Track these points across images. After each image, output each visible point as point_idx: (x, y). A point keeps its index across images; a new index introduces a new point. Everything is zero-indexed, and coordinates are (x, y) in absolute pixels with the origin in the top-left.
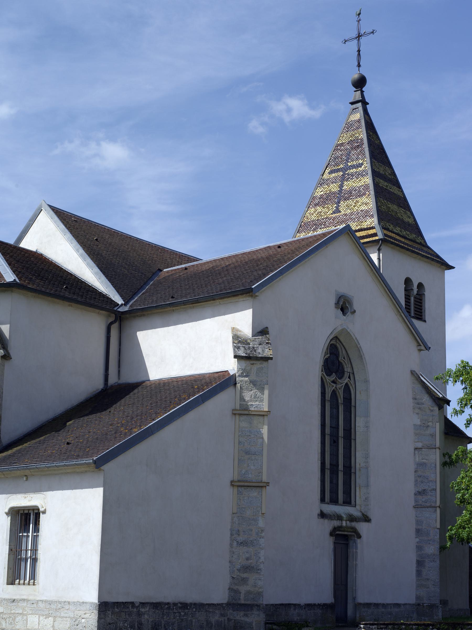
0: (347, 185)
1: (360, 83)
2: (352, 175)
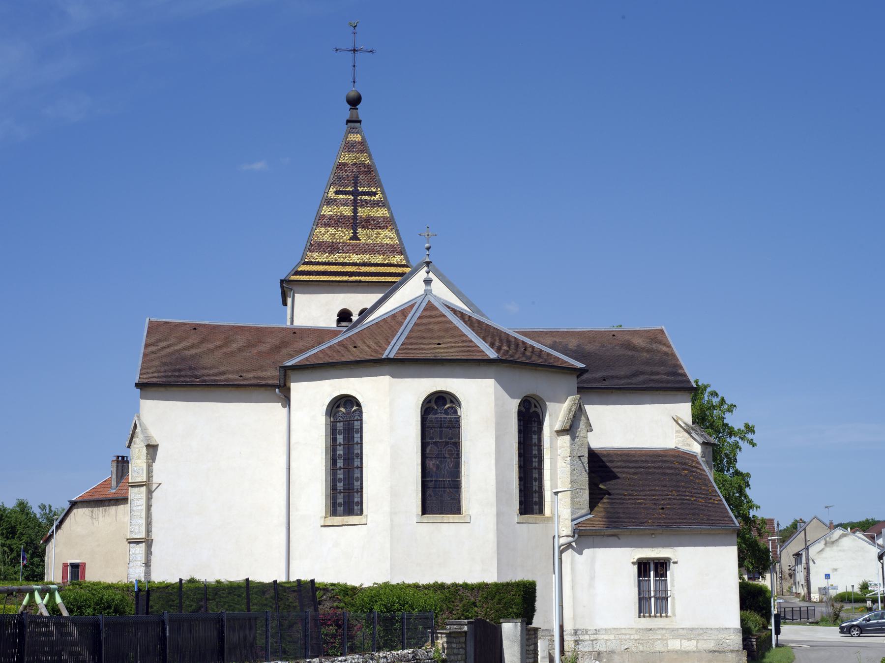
0: (362, 212)
1: (354, 102)
2: (367, 203)
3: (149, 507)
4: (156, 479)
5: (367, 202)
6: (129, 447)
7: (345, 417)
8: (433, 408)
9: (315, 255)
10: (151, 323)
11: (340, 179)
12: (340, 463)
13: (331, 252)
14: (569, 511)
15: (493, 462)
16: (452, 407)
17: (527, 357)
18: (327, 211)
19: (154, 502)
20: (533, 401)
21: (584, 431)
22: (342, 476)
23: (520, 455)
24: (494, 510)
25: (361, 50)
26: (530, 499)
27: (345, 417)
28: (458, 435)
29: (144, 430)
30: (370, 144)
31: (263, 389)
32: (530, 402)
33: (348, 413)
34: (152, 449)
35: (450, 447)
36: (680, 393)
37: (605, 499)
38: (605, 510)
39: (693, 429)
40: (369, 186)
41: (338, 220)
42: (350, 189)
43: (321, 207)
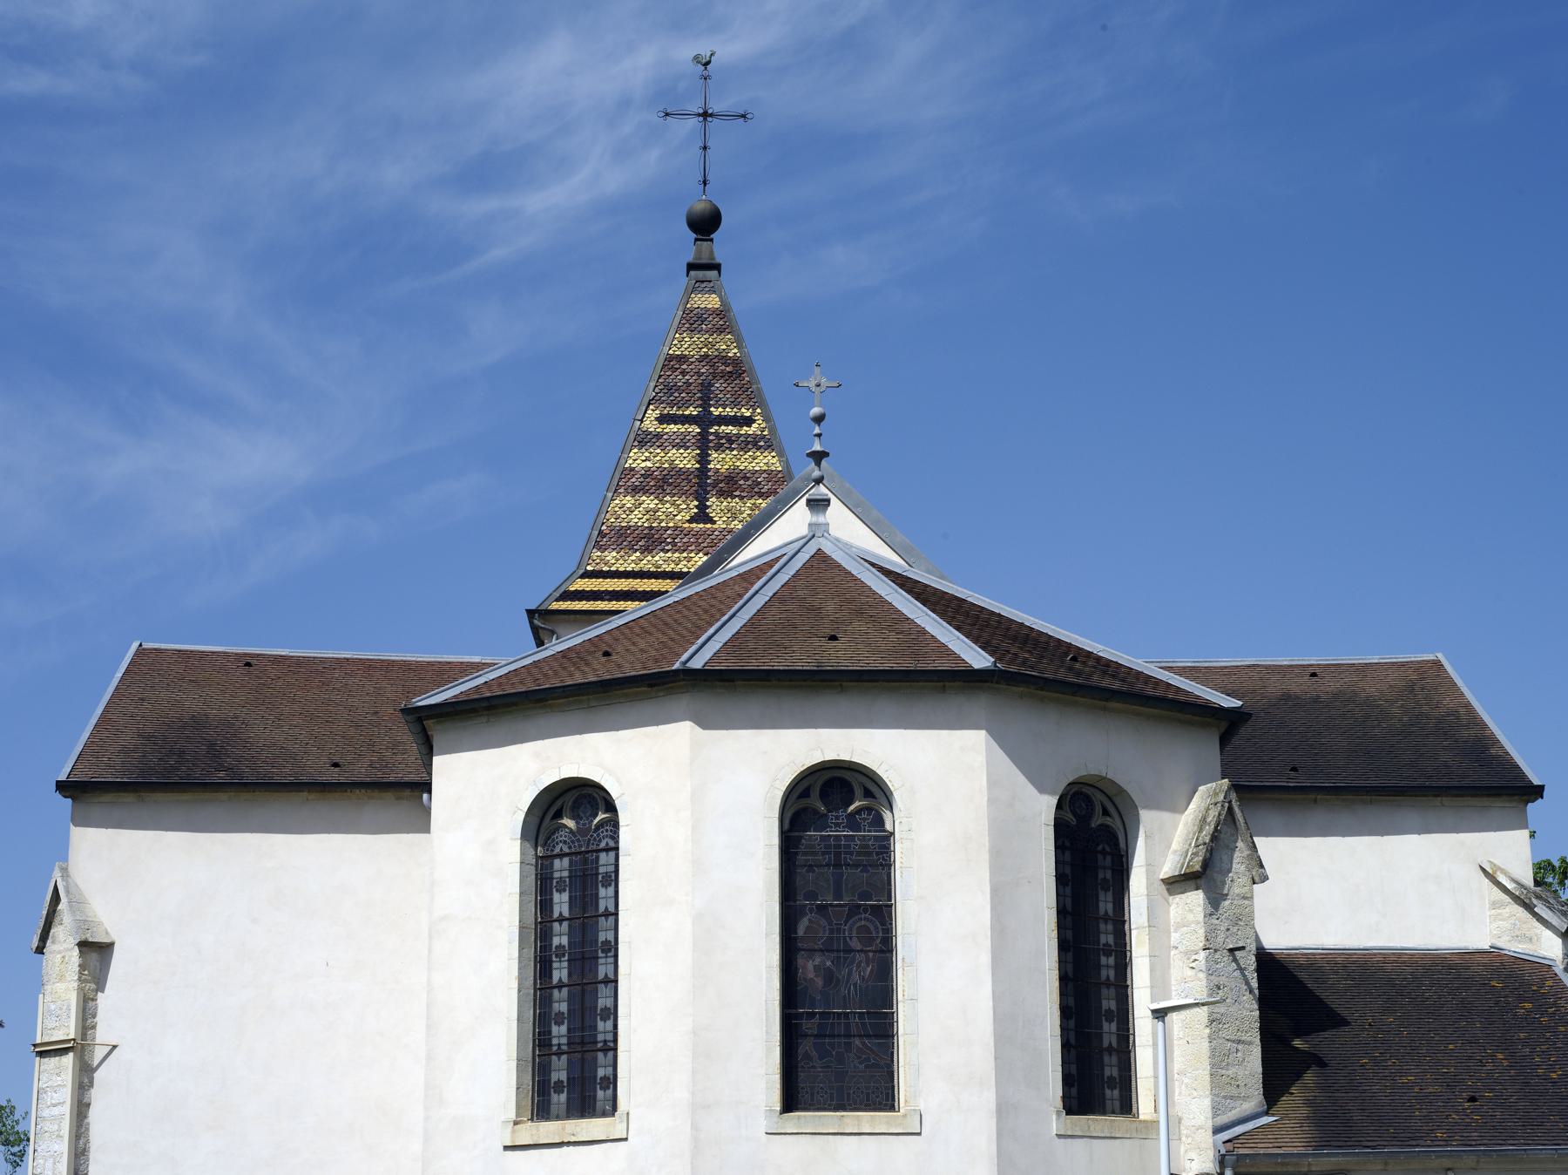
0: (720, 462)
1: (705, 224)
2: (730, 441)
3: (81, 1110)
4: (104, 1033)
5: (730, 439)
6: (40, 950)
7: (572, 838)
8: (816, 812)
9: (611, 556)
10: (141, 651)
11: (670, 389)
12: (560, 972)
13: (647, 550)
14: (1207, 1103)
15: (985, 958)
16: (869, 809)
17: (1079, 674)
18: (639, 460)
19: (97, 1096)
20: (1098, 797)
21: (1245, 880)
22: (564, 1007)
23: (1063, 946)
24: (989, 1097)
25: (711, 115)
26: (1095, 1072)
27: (572, 838)
28: (885, 887)
29: (78, 903)
30: (738, 308)
31: (389, 796)
32: (1088, 800)
33: (582, 831)
34: (96, 953)
35: (863, 920)
36: (1498, 803)
37: (1309, 1077)
38: (1309, 1103)
39: (1538, 897)
40: (735, 404)
41: (664, 480)
42: (692, 411)
43: (625, 450)
